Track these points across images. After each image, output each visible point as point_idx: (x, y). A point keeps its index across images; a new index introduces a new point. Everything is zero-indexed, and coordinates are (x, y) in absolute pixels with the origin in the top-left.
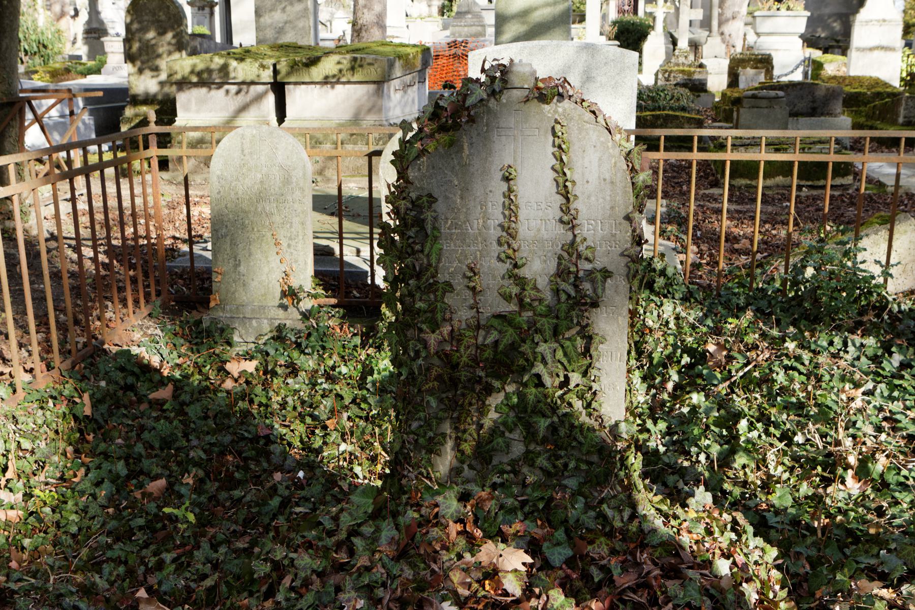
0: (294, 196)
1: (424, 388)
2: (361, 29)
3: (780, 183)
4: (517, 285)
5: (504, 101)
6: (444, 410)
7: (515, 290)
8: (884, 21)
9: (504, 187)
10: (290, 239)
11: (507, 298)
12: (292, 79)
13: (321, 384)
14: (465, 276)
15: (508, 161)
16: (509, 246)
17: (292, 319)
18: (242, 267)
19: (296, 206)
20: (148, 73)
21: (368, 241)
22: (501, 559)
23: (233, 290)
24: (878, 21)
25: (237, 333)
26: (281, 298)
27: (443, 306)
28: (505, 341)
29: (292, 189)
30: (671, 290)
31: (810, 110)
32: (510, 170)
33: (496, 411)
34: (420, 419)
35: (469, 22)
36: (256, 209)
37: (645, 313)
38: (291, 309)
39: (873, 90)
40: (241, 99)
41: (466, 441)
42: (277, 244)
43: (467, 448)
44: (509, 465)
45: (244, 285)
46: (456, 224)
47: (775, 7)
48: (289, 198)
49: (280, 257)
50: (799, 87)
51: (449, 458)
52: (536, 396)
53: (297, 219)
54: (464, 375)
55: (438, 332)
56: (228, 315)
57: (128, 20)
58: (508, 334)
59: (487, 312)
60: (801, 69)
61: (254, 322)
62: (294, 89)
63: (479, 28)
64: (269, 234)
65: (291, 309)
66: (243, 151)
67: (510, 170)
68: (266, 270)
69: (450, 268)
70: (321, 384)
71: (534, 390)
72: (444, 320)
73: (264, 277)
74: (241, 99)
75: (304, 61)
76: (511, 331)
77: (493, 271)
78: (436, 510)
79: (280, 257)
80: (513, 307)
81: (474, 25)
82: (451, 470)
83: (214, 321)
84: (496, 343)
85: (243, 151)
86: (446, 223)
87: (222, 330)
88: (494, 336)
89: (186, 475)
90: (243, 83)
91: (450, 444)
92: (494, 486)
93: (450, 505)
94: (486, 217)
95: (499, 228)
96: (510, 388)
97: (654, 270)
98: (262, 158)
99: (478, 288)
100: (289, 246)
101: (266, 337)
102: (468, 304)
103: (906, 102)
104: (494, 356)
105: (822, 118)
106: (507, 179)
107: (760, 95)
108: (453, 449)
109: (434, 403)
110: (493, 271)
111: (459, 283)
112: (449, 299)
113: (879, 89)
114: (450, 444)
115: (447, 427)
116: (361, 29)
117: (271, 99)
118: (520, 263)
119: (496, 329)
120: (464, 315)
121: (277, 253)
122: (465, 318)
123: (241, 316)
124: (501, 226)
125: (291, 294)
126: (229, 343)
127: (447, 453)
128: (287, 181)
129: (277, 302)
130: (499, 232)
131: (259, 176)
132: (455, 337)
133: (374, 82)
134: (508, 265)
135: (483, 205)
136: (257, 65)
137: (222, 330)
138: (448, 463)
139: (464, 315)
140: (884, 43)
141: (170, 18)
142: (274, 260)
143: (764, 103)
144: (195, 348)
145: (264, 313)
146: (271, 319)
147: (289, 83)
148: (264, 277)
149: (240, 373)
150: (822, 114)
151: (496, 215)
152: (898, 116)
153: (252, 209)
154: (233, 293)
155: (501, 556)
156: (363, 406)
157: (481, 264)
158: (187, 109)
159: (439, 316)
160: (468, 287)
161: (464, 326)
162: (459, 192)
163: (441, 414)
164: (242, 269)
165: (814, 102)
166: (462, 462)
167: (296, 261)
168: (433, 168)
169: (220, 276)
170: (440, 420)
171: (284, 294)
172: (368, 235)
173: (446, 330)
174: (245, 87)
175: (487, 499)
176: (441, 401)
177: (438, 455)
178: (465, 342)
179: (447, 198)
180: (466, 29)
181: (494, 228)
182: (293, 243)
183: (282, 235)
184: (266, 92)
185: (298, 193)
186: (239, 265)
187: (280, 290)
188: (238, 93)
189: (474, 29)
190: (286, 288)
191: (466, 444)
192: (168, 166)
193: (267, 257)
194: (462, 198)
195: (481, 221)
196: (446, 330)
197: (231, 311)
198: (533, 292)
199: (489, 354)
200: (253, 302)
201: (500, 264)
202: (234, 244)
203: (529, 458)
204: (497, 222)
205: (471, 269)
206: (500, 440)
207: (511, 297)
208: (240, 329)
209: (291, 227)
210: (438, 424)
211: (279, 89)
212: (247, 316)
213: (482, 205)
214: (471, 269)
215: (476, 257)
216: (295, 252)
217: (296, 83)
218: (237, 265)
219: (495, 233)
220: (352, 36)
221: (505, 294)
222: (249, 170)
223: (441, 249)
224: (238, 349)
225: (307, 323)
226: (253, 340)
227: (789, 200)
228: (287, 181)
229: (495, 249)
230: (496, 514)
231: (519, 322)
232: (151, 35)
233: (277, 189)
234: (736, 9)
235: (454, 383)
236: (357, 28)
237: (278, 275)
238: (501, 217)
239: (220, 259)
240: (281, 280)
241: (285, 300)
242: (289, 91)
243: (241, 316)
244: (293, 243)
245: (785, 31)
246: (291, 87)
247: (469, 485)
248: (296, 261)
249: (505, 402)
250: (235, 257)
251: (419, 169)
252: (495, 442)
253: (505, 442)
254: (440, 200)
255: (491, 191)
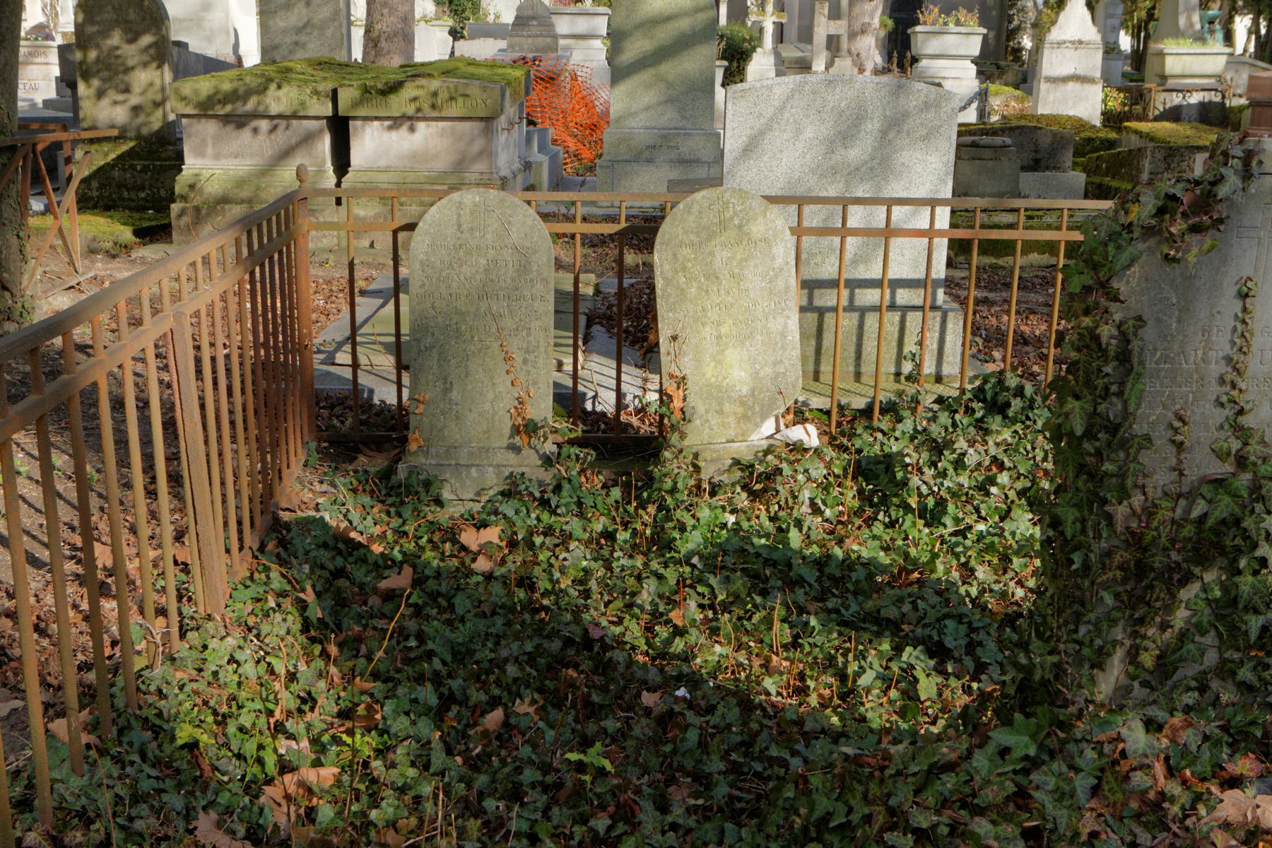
0: (534, 291)
1: (1100, 580)
2: (379, 37)
3: (1035, 263)
4: (1237, 438)
5: (1253, 191)
6: (1118, 609)
7: (1235, 445)
8: (1080, 42)
9: (1238, 305)
10: (527, 351)
11: (1221, 455)
12: (362, 112)
13: (618, 559)
14: (1171, 426)
15: (1247, 271)
16: (1234, 386)
17: (528, 464)
18: (455, 393)
19: (536, 304)
20: (113, 95)
21: (571, 350)
22: (1259, 811)
23: (440, 425)
24: (1073, 42)
25: (447, 487)
26: (512, 436)
27: (1138, 467)
28: (1217, 513)
29: (532, 280)
30: (1031, 415)
31: (1032, 163)
32: (1249, 284)
33: (1186, 608)
34: (1089, 622)
35: (534, 31)
36: (477, 309)
37: (1034, 449)
38: (526, 452)
39: (1082, 135)
40: (282, 138)
41: (1146, 650)
42: (508, 359)
43: (1147, 659)
44: (1194, 679)
45: (457, 418)
46: (1167, 356)
47: (941, 21)
48: (527, 293)
49: (512, 376)
50: (1017, 132)
51: (1116, 672)
52: (1253, 586)
53: (538, 323)
54: (1158, 561)
55: (1125, 503)
56: (433, 462)
57: (80, 19)
58: (1222, 504)
59: (1192, 475)
60: (975, 105)
61: (473, 470)
62: (363, 127)
63: (549, 40)
64: (496, 345)
65: (526, 452)
66: (459, 226)
67: (1249, 284)
68: (490, 396)
69: (1149, 416)
70: (618, 559)
71: (1250, 579)
72: (1136, 486)
73: (487, 406)
74: (282, 138)
75: (379, 86)
76: (1227, 499)
77: (1207, 421)
78: (1121, 746)
79: (512, 376)
80: (1228, 468)
81: (541, 36)
82: (1116, 690)
83: (412, 471)
84: (1204, 516)
85: (459, 226)
86: (1154, 354)
87: (427, 484)
88: (1199, 508)
89: (518, 701)
90: (280, 116)
91: (1119, 654)
92: (1187, 710)
93: (1136, 737)
94: (1208, 347)
95: (1223, 362)
96: (1209, 577)
97: (1008, 389)
98: (488, 236)
99: (1187, 444)
100: (525, 361)
101: (491, 493)
102: (1168, 464)
103: (1153, 153)
104: (1198, 534)
105: (1047, 173)
106: (1244, 296)
107: (982, 143)
108: (1122, 661)
109: (1109, 600)
110: (1207, 421)
111: (1161, 437)
112: (1146, 458)
113: (1088, 134)
114: (1119, 654)
115: (1118, 633)
116: (379, 37)
117: (325, 144)
118: (1247, 407)
119: (1204, 498)
120: (1161, 479)
121: (508, 372)
122: (1161, 483)
123: (453, 462)
124: (1229, 360)
125: (529, 429)
126: (439, 502)
127: (1113, 666)
128: (524, 268)
129: (505, 442)
130: (1223, 368)
131: (483, 261)
132: (1150, 510)
133: (481, 119)
134: (1228, 412)
135: (1206, 331)
136: (308, 91)
137: (427, 484)
138: (1113, 680)
139: (1161, 479)
140: (1080, 72)
141: (144, 19)
142: (503, 383)
143: (987, 153)
144: (392, 510)
145: (488, 458)
146: (498, 466)
147: (355, 118)
148: (487, 406)
149: (482, 546)
150: (1047, 168)
151: (1222, 344)
152: (1140, 171)
153: (473, 309)
154: (441, 430)
155: (1258, 806)
156: (700, 589)
157: (1193, 411)
158: (200, 153)
159: (1129, 482)
160: (1173, 442)
161: (1159, 493)
162: (1177, 313)
163: (1115, 614)
164: (455, 395)
165: (1036, 151)
166: (1133, 678)
167: (535, 383)
168: (1147, 280)
169: (422, 406)
170: (1113, 622)
171: (516, 430)
172: (571, 342)
173: (1137, 500)
174: (283, 123)
175: (1182, 728)
176: (1117, 596)
177: (1103, 670)
178: (1159, 516)
179: (1159, 321)
180: (530, 40)
181: (1216, 363)
182: (531, 357)
183: (515, 346)
184: (321, 131)
185: (539, 286)
186: (451, 389)
187: (510, 424)
188: (274, 129)
189: (541, 41)
190: (520, 420)
191: (1146, 654)
192: (170, 235)
193: (492, 378)
194: (1179, 321)
195: (1200, 353)
196: (1137, 500)
197: (438, 455)
198: (1259, 447)
199: (1189, 532)
200: (471, 442)
201: (1219, 410)
202: (443, 359)
203: (1226, 671)
204: (1221, 354)
205: (1181, 419)
206: (1191, 646)
207: (1229, 454)
208: (453, 481)
209: (528, 334)
210: (1110, 627)
211: (340, 129)
212: (461, 462)
213: (1204, 331)
214: (1181, 419)
215: (1186, 402)
216: (534, 371)
217: (366, 119)
218: (447, 391)
219: (1217, 368)
220: (365, 47)
221: (1221, 450)
222: (469, 253)
223: (1143, 391)
224: (451, 510)
225: (553, 471)
226: (472, 496)
227: (1054, 285)
228: (524, 268)
229: (1214, 390)
230: (1199, 747)
231: (1237, 488)
232: (116, 39)
233: (509, 280)
234: (867, 20)
235: (1141, 569)
236: (374, 35)
237: (508, 403)
238: (1228, 346)
239: (423, 381)
240: (513, 411)
241: (517, 438)
242: (356, 129)
243: (453, 462)
244: (531, 357)
245: (954, 53)
246: (359, 123)
247: (1148, 708)
248: (535, 383)
249: (1204, 596)
250: (445, 379)
251: (1128, 282)
252: (1185, 649)
253: (1199, 649)
254: (1150, 323)
255: (1219, 312)
